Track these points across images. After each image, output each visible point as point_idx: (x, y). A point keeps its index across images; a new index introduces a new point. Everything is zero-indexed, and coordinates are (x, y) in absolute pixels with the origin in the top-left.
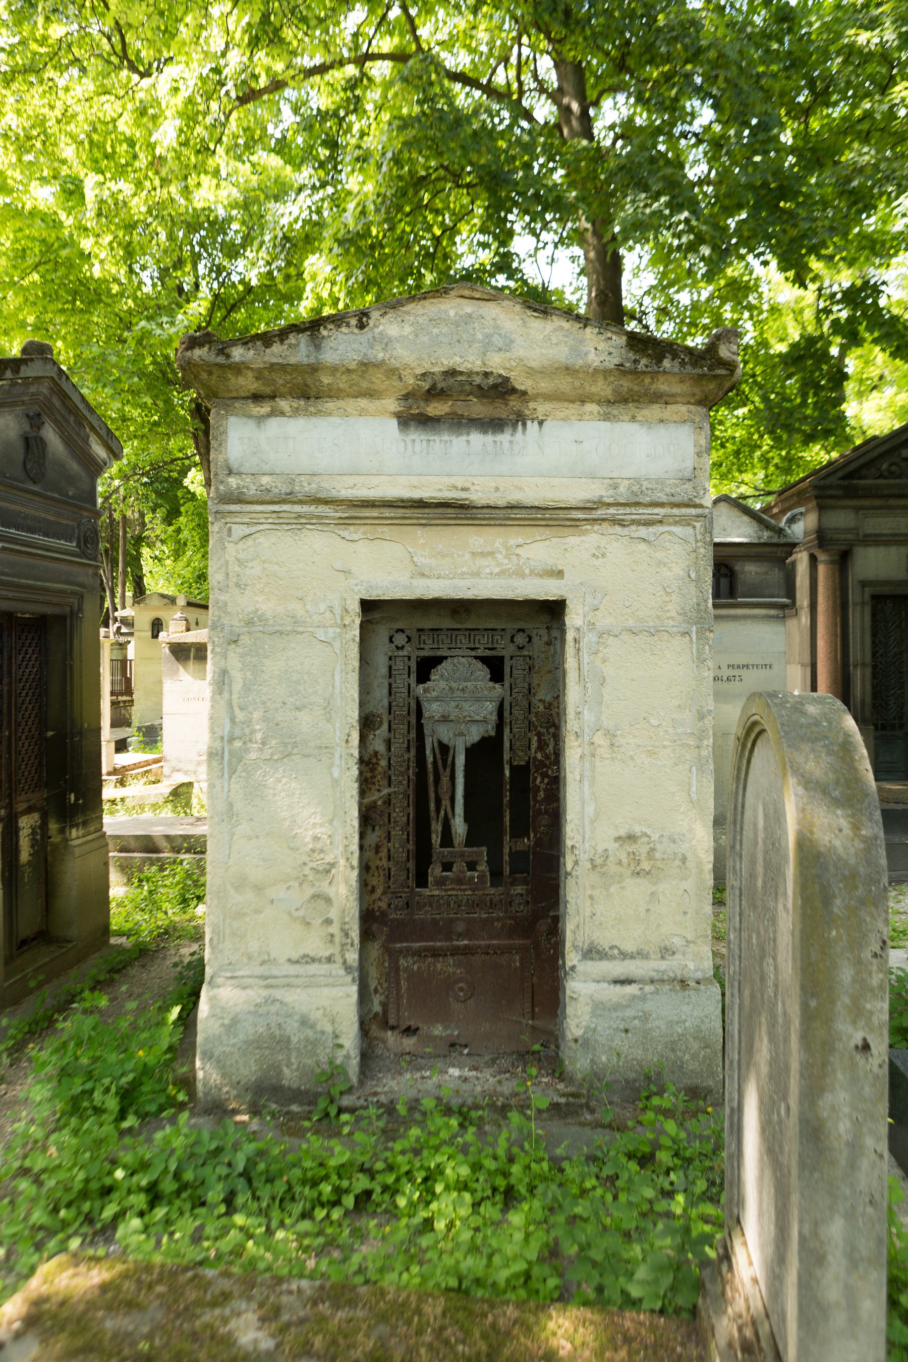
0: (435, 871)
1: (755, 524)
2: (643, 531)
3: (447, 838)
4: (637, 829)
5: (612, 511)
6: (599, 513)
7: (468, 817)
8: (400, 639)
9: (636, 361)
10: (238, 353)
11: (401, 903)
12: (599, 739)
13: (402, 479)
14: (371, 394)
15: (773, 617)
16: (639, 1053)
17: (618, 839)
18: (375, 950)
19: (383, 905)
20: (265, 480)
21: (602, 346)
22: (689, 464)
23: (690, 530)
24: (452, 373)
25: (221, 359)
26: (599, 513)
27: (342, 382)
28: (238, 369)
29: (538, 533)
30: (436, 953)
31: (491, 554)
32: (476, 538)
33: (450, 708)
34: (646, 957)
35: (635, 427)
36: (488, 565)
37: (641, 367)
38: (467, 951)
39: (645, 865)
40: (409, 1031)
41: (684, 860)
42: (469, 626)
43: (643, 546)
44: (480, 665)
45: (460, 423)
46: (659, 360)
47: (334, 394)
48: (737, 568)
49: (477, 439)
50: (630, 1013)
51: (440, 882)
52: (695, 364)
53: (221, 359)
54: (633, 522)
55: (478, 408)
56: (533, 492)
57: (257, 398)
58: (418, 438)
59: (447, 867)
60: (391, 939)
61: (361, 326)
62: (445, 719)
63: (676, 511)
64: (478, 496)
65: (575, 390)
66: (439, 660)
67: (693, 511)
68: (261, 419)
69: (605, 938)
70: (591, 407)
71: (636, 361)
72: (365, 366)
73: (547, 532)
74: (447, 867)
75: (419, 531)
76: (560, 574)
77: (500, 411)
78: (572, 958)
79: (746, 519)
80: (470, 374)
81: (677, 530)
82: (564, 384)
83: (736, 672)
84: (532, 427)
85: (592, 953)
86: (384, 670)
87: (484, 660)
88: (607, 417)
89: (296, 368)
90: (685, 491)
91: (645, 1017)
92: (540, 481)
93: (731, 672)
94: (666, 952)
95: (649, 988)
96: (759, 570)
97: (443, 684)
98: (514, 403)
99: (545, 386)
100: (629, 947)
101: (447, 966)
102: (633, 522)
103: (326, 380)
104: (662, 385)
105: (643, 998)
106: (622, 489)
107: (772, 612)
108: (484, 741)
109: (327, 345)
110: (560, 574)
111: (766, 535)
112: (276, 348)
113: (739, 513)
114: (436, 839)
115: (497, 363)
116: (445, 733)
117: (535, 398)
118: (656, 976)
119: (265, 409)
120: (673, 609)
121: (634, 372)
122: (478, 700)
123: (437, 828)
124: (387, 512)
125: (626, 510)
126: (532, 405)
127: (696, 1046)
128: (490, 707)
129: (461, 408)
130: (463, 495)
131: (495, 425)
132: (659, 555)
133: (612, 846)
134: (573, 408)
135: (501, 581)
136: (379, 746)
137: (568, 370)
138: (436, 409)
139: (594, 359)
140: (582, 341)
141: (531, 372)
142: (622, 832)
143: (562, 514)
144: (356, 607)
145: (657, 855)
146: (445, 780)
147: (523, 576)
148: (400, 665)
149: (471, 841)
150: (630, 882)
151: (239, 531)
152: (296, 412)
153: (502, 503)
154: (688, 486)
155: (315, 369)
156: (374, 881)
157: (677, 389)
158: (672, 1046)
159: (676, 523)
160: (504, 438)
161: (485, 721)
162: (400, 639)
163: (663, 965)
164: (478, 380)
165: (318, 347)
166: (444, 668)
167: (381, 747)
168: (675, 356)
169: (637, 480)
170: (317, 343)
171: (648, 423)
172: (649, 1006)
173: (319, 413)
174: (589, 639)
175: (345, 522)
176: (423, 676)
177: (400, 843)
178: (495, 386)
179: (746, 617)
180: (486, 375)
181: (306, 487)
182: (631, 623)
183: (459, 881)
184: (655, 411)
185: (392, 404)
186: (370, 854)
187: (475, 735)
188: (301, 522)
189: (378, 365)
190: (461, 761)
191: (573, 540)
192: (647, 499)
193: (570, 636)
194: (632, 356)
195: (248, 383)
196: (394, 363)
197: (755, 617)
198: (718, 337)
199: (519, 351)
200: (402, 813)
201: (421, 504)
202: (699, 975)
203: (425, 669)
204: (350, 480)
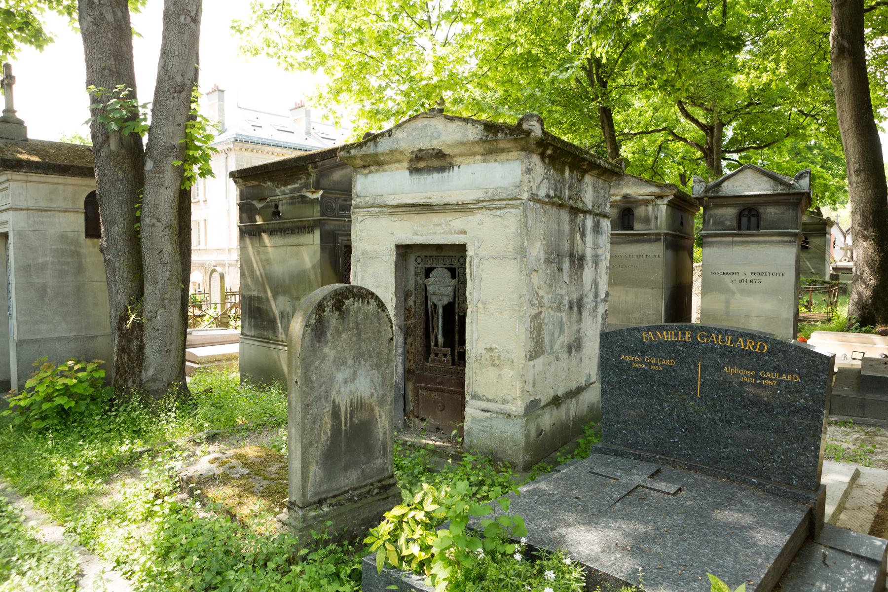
0: (432, 356)
1: (772, 182)
2: (498, 212)
3: (436, 345)
4: (494, 346)
5: (485, 204)
6: (479, 205)
7: (444, 335)
8: (419, 260)
9: (487, 136)
10: (353, 152)
11: (419, 367)
12: (479, 305)
13: (410, 195)
14: (399, 161)
15: (786, 242)
16: (489, 442)
17: (486, 349)
18: (410, 386)
19: (413, 367)
20: (367, 199)
21: (474, 131)
22: (519, 180)
23: (518, 210)
24: (420, 150)
25: (348, 155)
26: (479, 205)
27: (387, 158)
28: (354, 157)
29: (458, 215)
30: (431, 390)
31: (440, 225)
32: (435, 218)
33: (436, 289)
34: (496, 402)
35: (497, 164)
36: (439, 230)
37: (489, 139)
38: (441, 390)
39: (497, 362)
40: (423, 420)
41: (512, 361)
42: (442, 254)
43: (499, 219)
44: (446, 271)
45: (430, 170)
46: (496, 134)
47: (387, 163)
48: (761, 210)
49: (436, 176)
50: (486, 424)
51: (433, 361)
52: (511, 134)
53: (348, 155)
54: (494, 208)
55: (436, 163)
56: (455, 197)
57: (364, 167)
58: (415, 177)
59: (436, 355)
60: (416, 382)
61: (390, 136)
62: (434, 294)
63: (511, 202)
64: (434, 201)
65: (469, 150)
66: (433, 269)
67: (518, 202)
68: (366, 175)
69: (481, 391)
70: (479, 157)
71: (487, 136)
72: (392, 151)
73: (461, 214)
74: (436, 355)
75: (416, 216)
76: (465, 232)
77: (444, 163)
78: (468, 398)
79: (765, 178)
80: (427, 150)
81: (512, 210)
82: (463, 149)
83: (757, 277)
84: (456, 168)
85: (475, 397)
86: (413, 273)
87: (449, 269)
88: (485, 161)
89: (370, 155)
90: (515, 192)
91: (491, 427)
92: (458, 192)
93: (753, 277)
94: (505, 401)
95: (494, 415)
96: (777, 211)
97: (433, 279)
98: (448, 159)
99: (456, 151)
100: (490, 397)
101: (435, 396)
102: (494, 208)
103: (382, 158)
104: (502, 145)
105: (491, 419)
106: (489, 194)
107: (786, 239)
108: (449, 303)
109: (379, 145)
110: (465, 232)
111: (780, 189)
112: (364, 148)
113: (760, 175)
114: (432, 344)
115: (436, 144)
116: (434, 299)
117: (455, 156)
118: (499, 411)
119: (367, 171)
120: (511, 247)
121: (486, 141)
122: (446, 286)
123: (432, 338)
124: (404, 209)
125: (491, 203)
126: (455, 159)
127: (511, 444)
128: (450, 289)
129: (430, 164)
130: (428, 201)
131: (442, 169)
132: (505, 223)
133: (484, 352)
134: (471, 159)
135: (443, 236)
136: (411, 303)
137: (462, 143)
138: (421, 165)
139: (471, 137)
140: (466, 130)
141: (449, 146)
142: (488, 347)
143: (465, 206)
144: (394, 248)
145: (502, 358)
146: (435, 319)
147: (452, 234)
148: (419, 271)
149: (445, 345)
150: (491, 368)
151: (360, 219)
152: (377, 171)
153: (442, 203)
154: (517, 190)
155: (376, 155)
156: (410, 357)
157: (508, 145)
158: (502, 442)
159: (512, 208)
160: (445, 174)
161: (448, 295)
162: (419, 260)
163: (502, 407)
164: (431, 152)
165: (376, 146)
166: (435, 271)
167: (412, 304)
168: (503, 131)
169: (496, 189)
170: (376, 145)
171: (501, 162)
172: (493, 423)
173: (383, 170)
174: (476, 261)
175: (392, 214)
176: (427, 276)
177: (420, 343)
178: (437, 154)
179: (766, 242)
180: (433, 149)
181: (379, 201)
182: (493, 253)
183: (440, 362)
184: (504, 156)
185: (406, 165)
186: (408, 346)
187: (445, 301)
188: (378, 214)
189: (396, 150)
190: (440, 311)
191: (471, 217)
192: (498, 198)
193: (468, 259)
194: (486, 134)
195: (359, 162)
196: (401, 149)
197: (773, 242)
198: (522, 120)
199: (443, 138)
200: (420, 331)
201: (413, 205)
202: (516, 414)
203: (428, 272)
204: (393, 197)
